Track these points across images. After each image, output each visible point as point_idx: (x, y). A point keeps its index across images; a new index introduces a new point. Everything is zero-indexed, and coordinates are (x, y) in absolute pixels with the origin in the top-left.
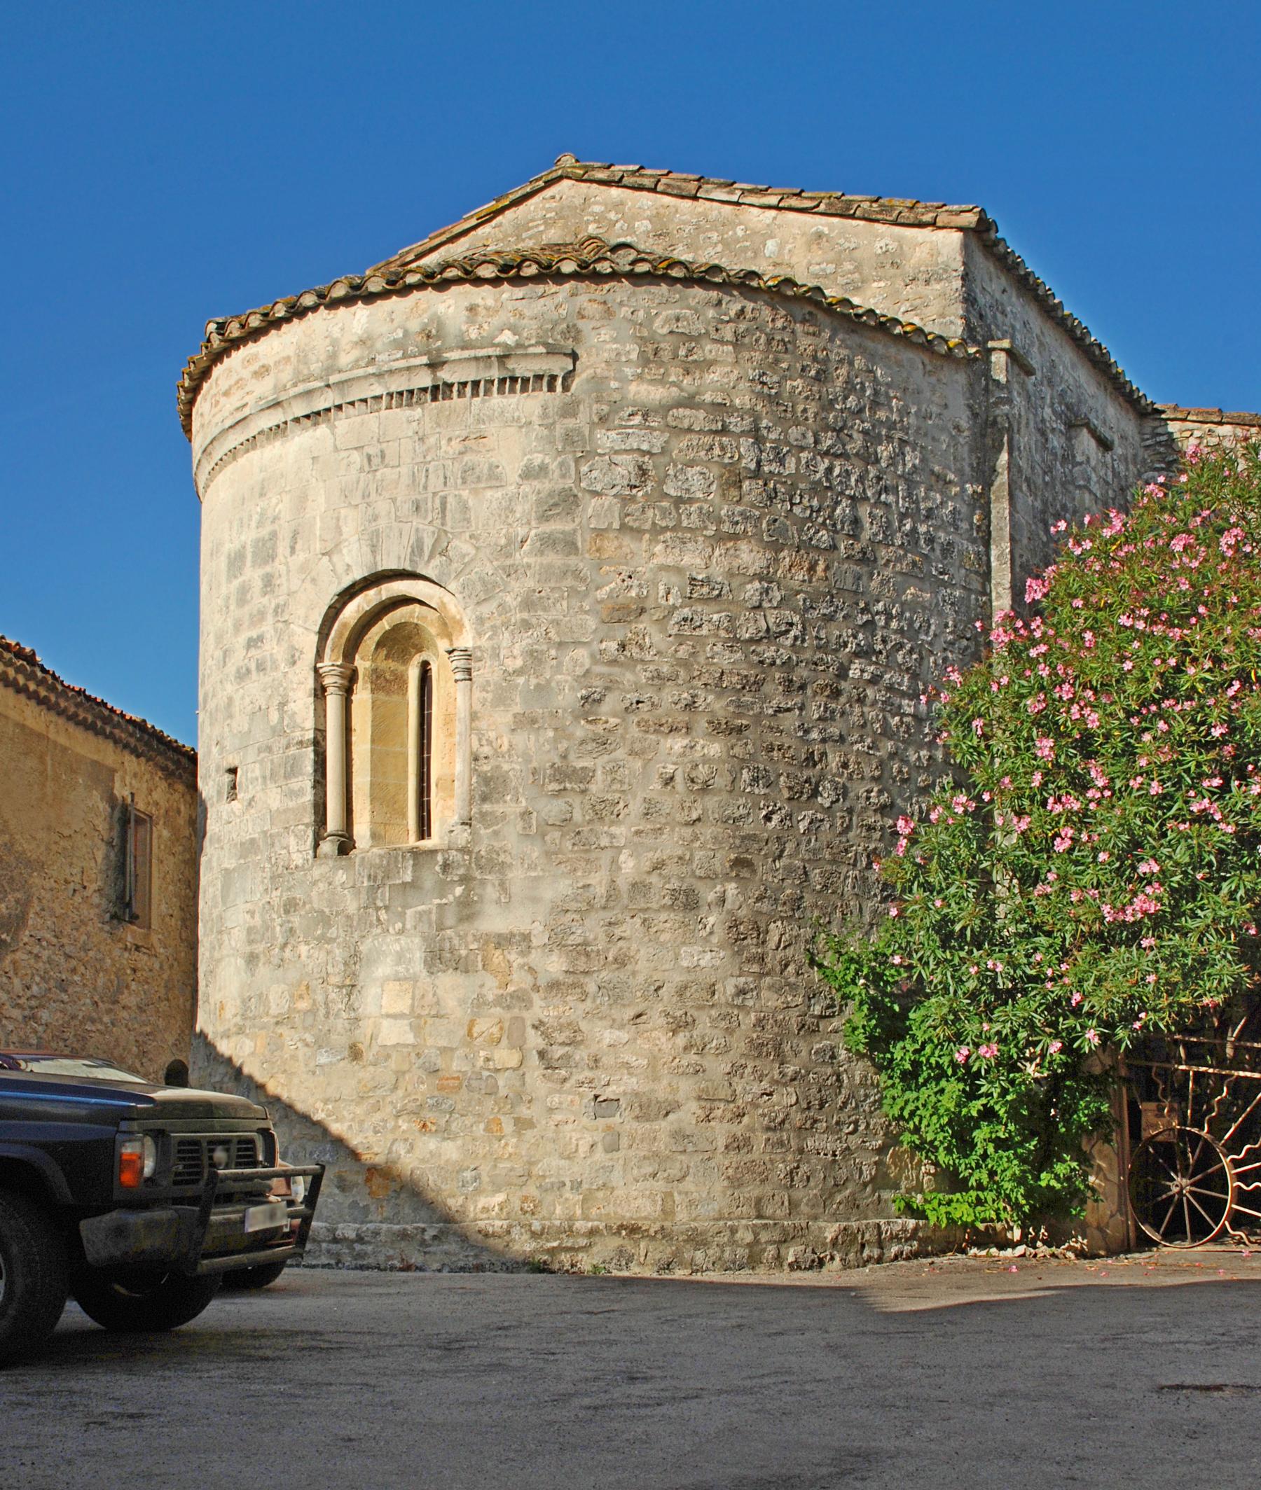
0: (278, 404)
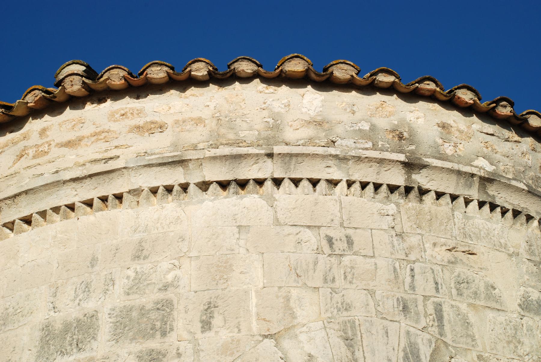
0: (181, 162)
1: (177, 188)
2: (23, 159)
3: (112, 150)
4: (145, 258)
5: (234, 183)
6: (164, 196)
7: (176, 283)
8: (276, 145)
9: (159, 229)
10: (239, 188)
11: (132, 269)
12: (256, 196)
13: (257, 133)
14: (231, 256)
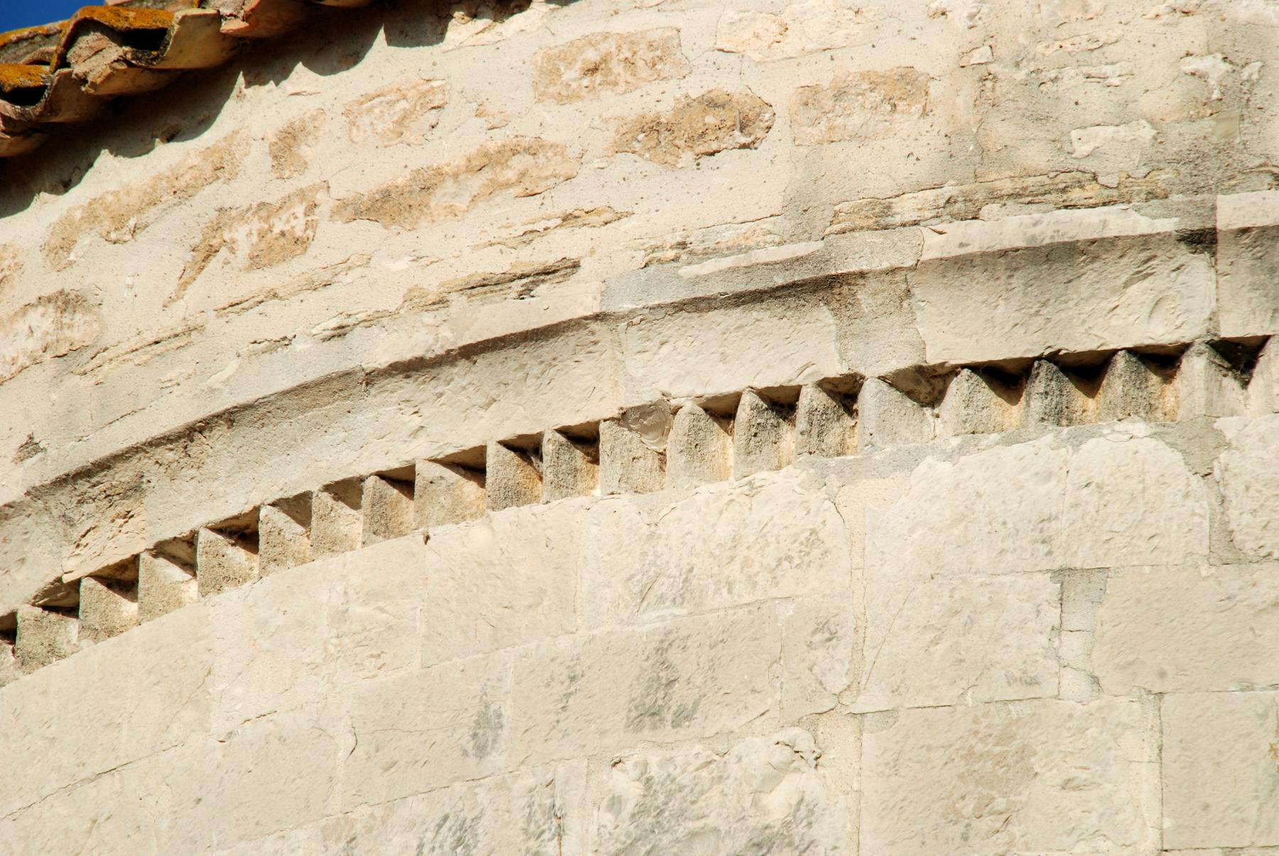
0: (825, 287)
1: (811, 399)
2: (214, 263)
3: (551, 236)
4: (683, 717)
5: (1045, 369)
6: (763, 435)
7: (801, 829)
8: (1232, 189)
9: (738, 588)
10: (1070, 387)
11: (629, 764)
12: (1139, 427)
13: (1147, 133)
14: (1026, 709)
